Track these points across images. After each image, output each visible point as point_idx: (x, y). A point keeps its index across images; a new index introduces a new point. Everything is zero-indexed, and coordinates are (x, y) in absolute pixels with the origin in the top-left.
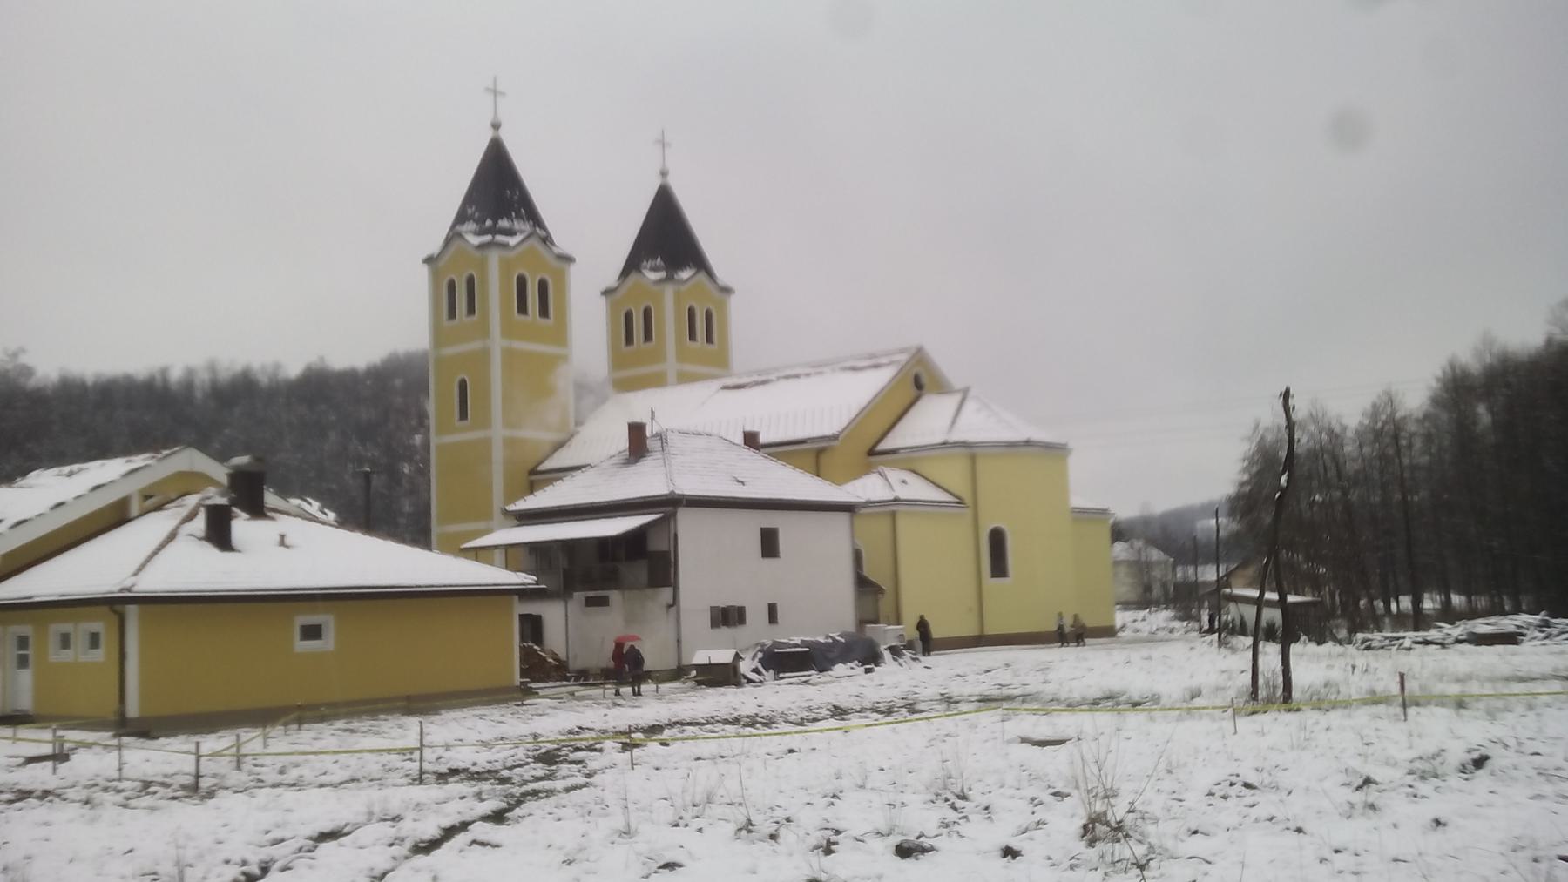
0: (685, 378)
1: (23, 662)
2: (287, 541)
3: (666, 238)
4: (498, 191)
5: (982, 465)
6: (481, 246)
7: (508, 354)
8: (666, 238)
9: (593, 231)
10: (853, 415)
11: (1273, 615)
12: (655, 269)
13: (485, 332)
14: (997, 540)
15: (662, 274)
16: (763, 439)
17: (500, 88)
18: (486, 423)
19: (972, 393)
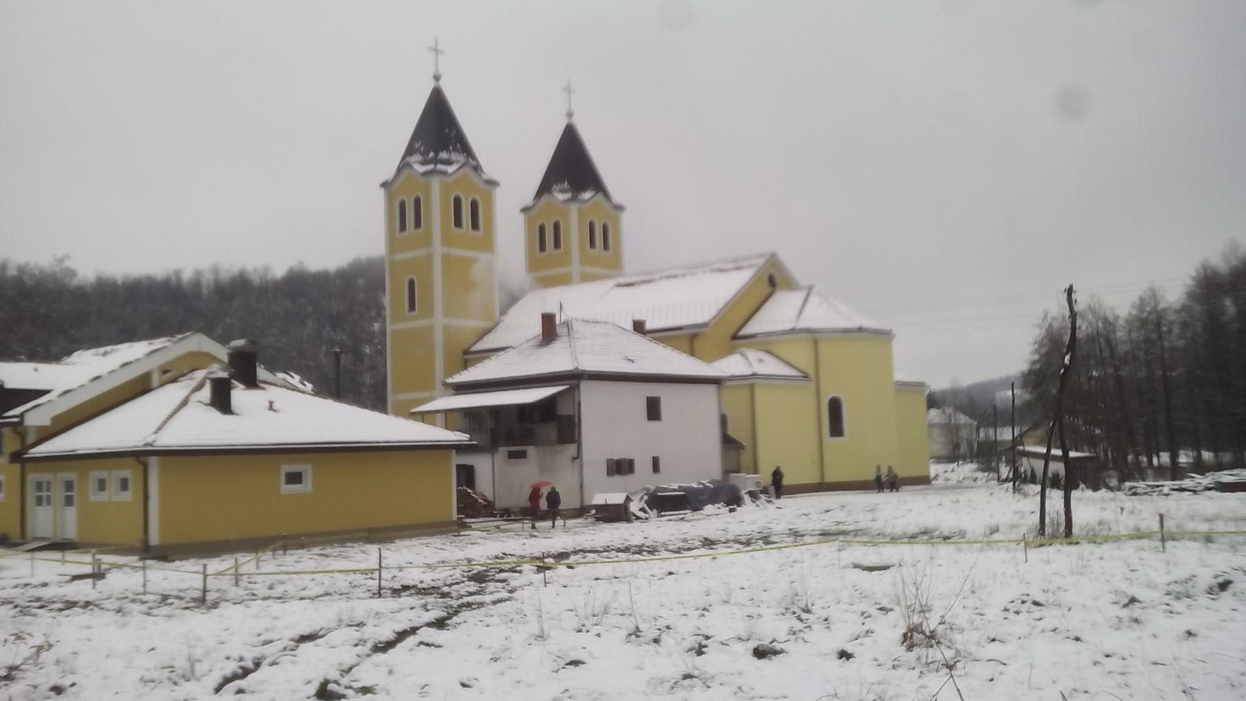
0: (587, 278)
1: (69, 501)
2: (275, 406)
3: (571, 166)
4: (439, 130)
5: (823, 347)
6: (426, 174)
7: (447, 259)
8: (571, 166)
9: (512, 160)
10: (721, 305)
11: (1058, 468)
12: (563, 191)
13: (427, 241)
14: (835, 407)
15: (568, 196)
16: (648, 326)
17: (439, 47)
18: (429, 313)
19: (816, 289)
